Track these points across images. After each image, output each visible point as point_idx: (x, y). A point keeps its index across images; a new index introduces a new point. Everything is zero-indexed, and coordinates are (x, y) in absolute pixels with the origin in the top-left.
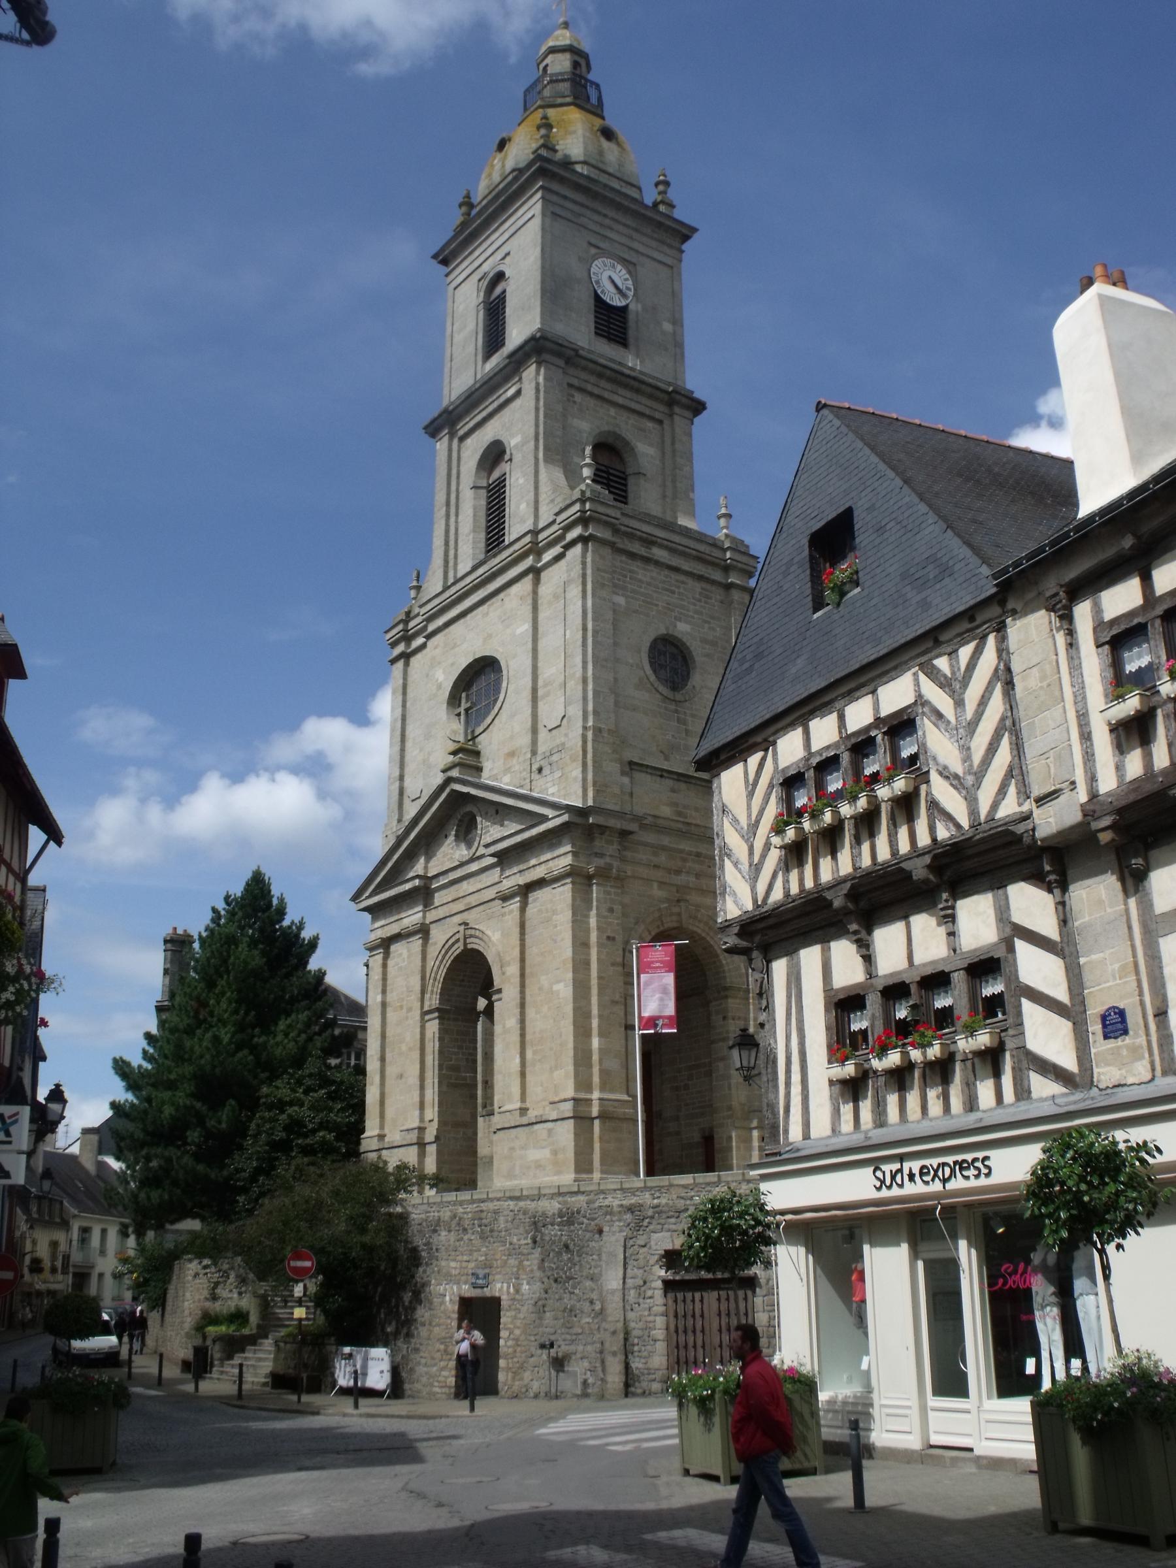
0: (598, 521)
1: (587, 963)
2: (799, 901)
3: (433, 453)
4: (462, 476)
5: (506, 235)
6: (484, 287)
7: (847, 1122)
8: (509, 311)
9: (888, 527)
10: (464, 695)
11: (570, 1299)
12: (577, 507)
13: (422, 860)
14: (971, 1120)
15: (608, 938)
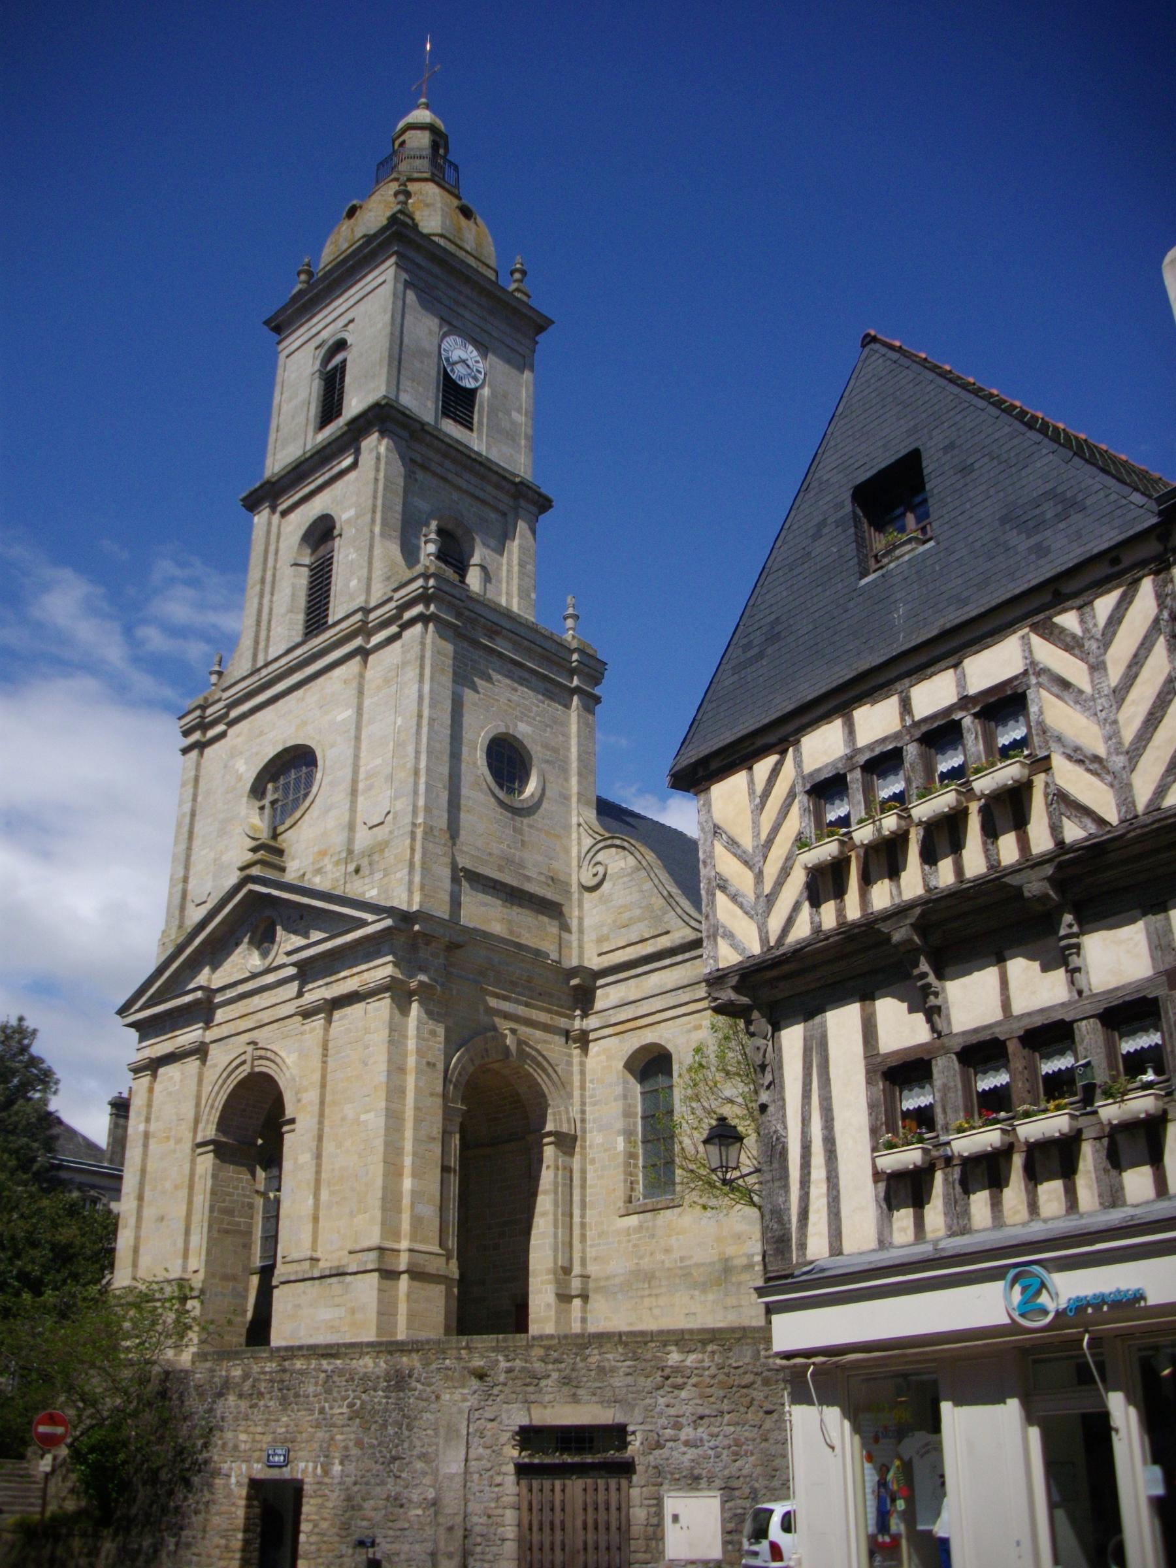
1: (402, 1091)
2: (837, 938)
3: (250, 526)
4: (280, 553)
7: (903, 1230)
8: (348, 379)
9: (977, 465)
10: (270, 786)
11: (395, 1484)
12: (420, 582)
13: (207, 970)
14: (1115, 1216)
15: (428, 1064)
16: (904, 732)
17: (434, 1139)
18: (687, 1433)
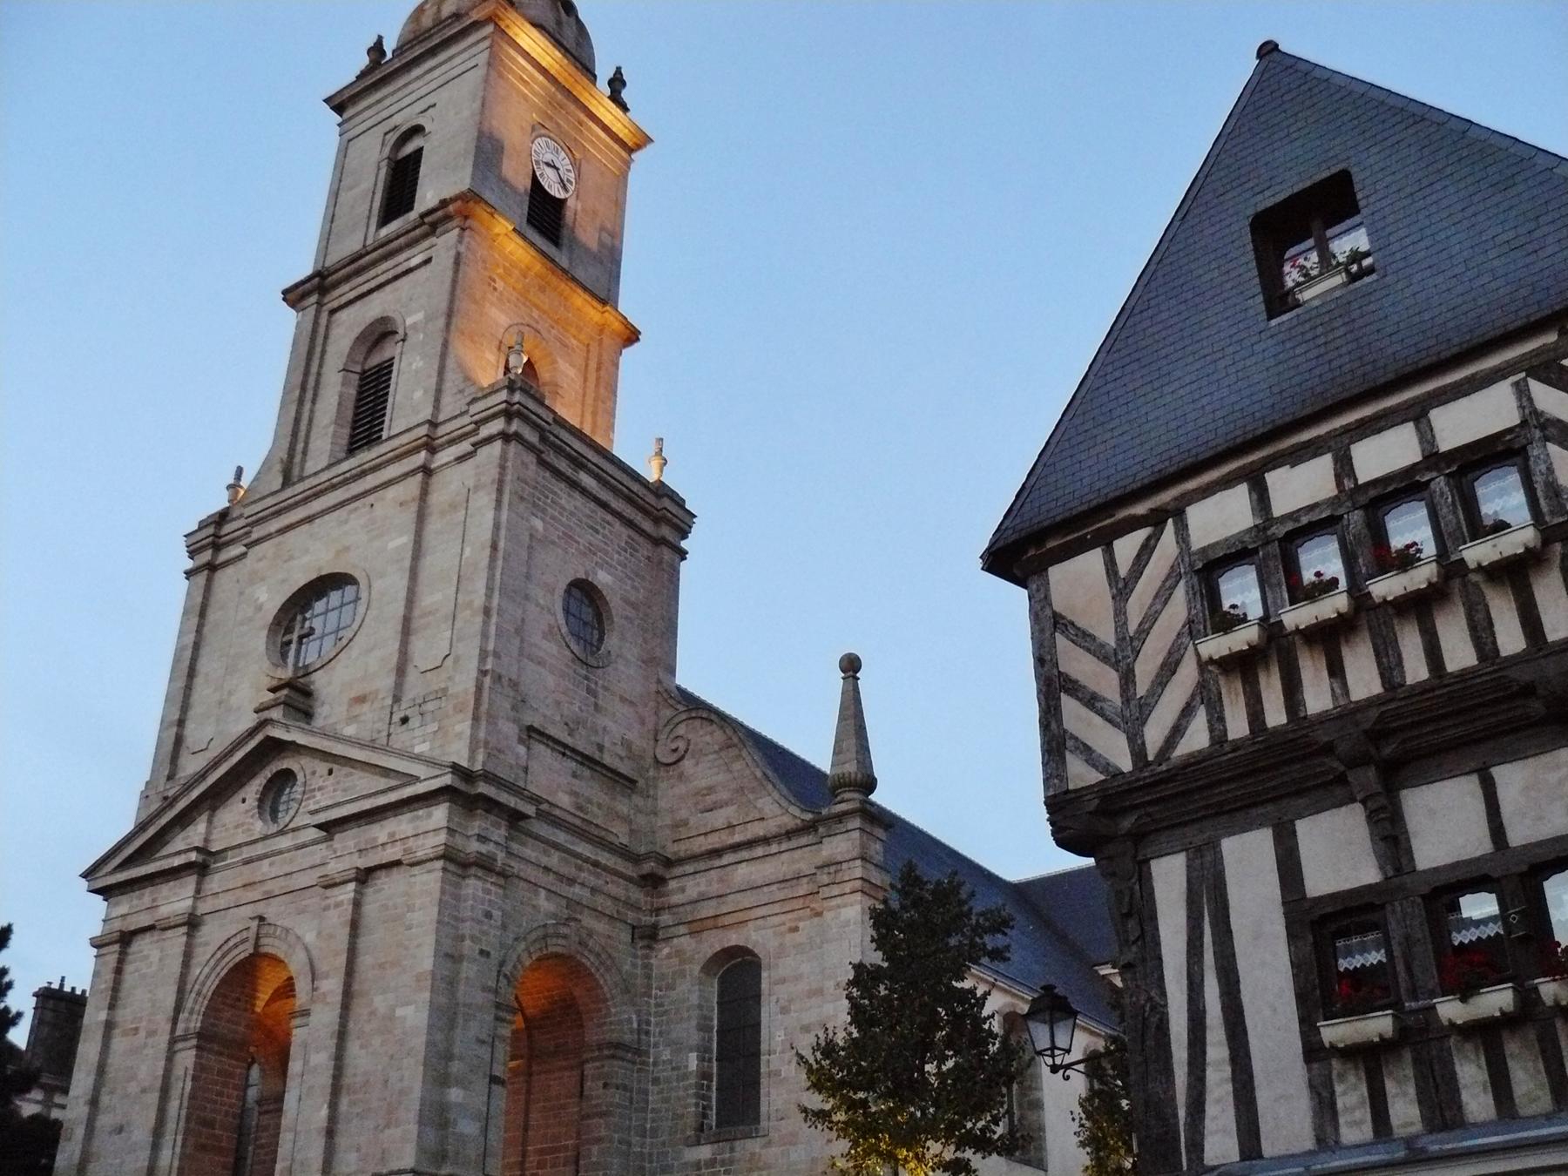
0: (525, 419)
5: (433, 85)
6: (392, 142)
8: (424, 169)
12: (503, 395)
15: (482, 952)
16: (1343, 498)
17: (483, 1042)
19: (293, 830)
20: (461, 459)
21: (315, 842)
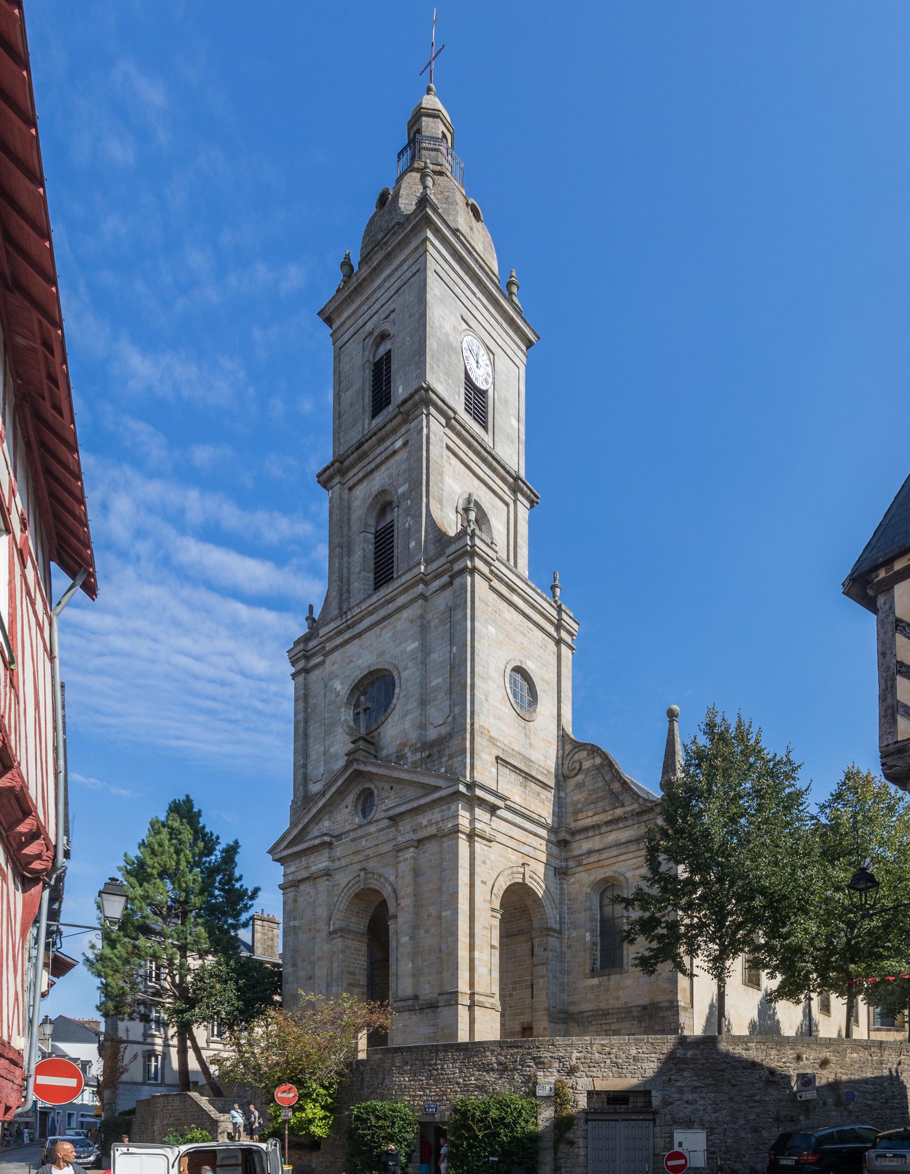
8: (394, 367)
18: (688, 1096)
19: (376, 821)
20: (443, 588)
21: (388, 827)
